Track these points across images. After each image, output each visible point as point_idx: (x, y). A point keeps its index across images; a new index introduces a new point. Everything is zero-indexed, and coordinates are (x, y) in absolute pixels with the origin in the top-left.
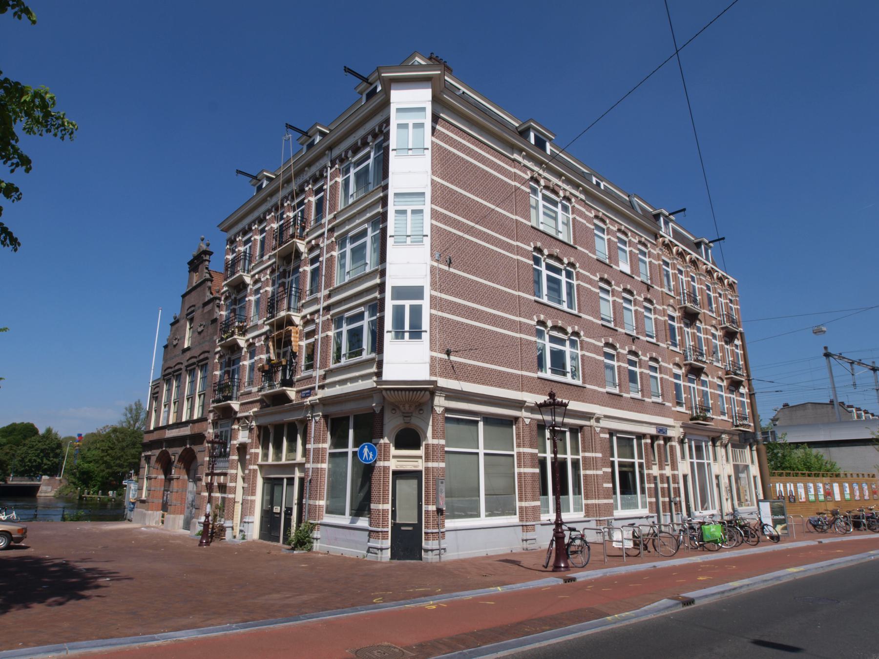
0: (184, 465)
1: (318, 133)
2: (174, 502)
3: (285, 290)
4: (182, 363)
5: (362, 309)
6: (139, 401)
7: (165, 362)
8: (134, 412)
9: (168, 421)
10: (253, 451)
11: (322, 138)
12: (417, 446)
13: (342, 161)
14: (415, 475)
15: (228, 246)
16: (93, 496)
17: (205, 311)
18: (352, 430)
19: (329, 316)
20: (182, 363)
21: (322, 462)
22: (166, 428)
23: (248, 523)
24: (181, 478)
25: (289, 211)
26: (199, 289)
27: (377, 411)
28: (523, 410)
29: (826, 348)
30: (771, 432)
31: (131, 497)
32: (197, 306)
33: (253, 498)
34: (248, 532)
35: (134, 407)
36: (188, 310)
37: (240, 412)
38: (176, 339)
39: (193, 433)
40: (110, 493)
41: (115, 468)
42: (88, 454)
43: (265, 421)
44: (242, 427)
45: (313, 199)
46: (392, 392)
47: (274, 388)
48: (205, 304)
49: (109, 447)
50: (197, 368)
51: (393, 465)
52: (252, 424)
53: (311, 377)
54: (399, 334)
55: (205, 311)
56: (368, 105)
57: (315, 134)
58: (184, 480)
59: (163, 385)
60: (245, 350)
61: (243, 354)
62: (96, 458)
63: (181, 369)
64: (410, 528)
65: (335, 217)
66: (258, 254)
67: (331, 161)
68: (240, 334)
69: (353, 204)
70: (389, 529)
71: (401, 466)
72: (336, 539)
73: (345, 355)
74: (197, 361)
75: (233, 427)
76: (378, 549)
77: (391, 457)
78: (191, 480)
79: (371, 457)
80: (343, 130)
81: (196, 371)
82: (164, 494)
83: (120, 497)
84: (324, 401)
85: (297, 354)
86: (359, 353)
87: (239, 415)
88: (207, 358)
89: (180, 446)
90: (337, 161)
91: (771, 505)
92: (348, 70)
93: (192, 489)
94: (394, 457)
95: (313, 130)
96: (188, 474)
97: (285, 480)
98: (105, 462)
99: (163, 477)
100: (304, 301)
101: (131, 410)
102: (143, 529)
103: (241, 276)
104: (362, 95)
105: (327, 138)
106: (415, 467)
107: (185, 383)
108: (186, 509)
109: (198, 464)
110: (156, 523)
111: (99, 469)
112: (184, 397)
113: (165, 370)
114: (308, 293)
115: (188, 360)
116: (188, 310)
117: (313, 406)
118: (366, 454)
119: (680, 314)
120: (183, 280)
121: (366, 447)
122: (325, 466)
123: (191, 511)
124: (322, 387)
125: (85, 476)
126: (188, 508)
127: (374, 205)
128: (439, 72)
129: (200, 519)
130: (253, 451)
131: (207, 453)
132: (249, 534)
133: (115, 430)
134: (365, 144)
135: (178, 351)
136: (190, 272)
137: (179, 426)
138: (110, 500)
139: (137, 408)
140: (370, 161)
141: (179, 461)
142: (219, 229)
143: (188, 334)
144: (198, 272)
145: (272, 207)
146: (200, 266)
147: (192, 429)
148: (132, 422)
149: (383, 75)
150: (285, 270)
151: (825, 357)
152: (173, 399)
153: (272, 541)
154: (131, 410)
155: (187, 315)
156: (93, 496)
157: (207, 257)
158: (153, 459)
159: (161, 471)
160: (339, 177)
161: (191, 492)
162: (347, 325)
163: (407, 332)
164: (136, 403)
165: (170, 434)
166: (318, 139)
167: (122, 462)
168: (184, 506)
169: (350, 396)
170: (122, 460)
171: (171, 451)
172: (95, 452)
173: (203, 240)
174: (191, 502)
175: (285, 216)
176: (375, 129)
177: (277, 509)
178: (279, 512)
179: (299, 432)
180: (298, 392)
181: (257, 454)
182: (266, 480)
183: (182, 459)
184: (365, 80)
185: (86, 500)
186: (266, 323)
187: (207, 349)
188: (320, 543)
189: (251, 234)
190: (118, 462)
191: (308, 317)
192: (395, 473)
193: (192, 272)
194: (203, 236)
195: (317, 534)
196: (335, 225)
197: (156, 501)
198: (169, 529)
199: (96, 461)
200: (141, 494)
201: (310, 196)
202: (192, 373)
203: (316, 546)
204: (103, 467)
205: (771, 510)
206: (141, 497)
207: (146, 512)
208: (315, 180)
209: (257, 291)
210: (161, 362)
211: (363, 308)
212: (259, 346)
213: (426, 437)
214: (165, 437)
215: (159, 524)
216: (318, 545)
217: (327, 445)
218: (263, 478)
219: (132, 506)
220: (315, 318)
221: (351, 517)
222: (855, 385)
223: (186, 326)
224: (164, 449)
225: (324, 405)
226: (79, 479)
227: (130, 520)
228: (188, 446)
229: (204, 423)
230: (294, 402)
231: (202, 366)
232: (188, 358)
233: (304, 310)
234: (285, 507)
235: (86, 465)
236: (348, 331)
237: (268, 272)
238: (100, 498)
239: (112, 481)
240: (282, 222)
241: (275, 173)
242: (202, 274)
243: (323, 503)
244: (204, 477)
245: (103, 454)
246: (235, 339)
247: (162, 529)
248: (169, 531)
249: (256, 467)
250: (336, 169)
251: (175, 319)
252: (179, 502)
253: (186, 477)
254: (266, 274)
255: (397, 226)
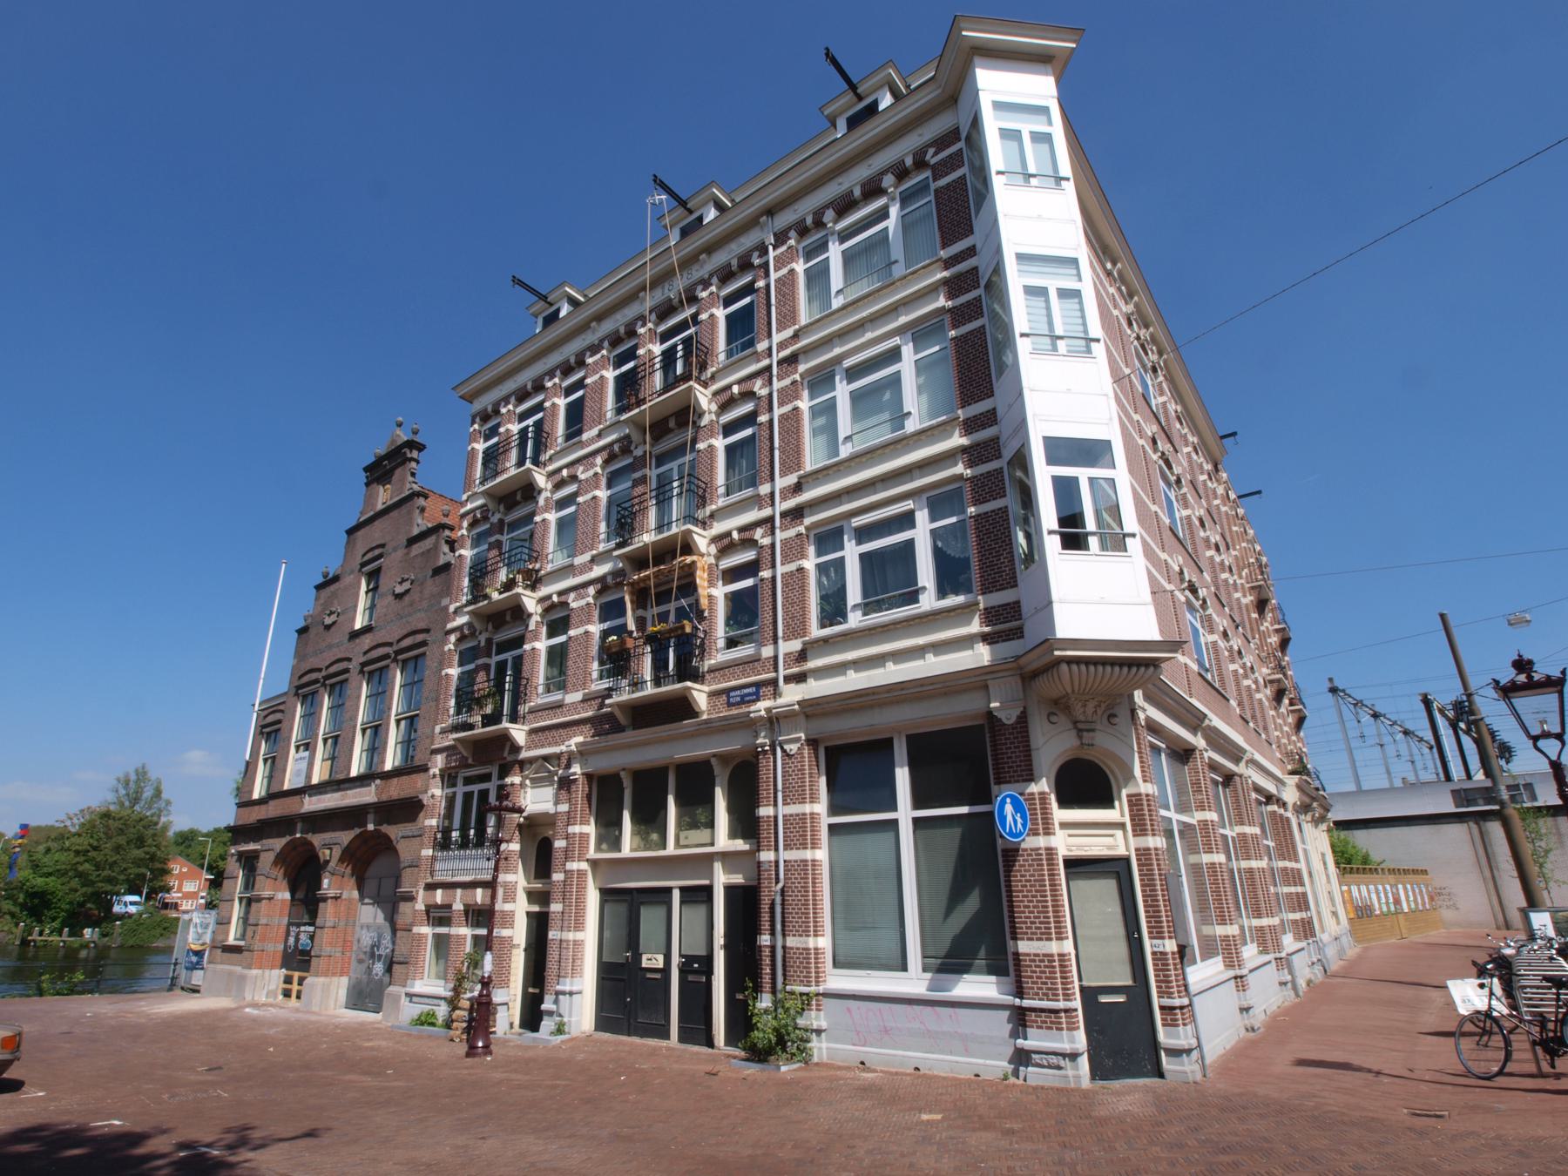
0: (353, 870)
1: (566, 299)
2: (327, 950)
3: (501, 554)
4: (349, 660)
5: (908, 505)
6: (143, 768)
7: (299, 662)
8: (132, 785)
9: (309, 776)
10: (575, 829)
11: (572, 309)
12: (1106, 800)
13: (803, 232)
14: (1114, 868)
15: (476, 426)
16: (50, 939)
17: (412, 554)
18: (906, 769)
19: (802, 529)
20: (349, 660)
21: (814, 846)
22: (304, 792)
23: (571, 994)
24: (344, 897)
25: (651, 341)
26: (395, 514)
27: (1009, 717)
28: (1199, 734)
29: (1331, 680)
30: (1524, 785)
31: (190, 940)
32: (389, 548)
33: (579, 936)
34: (570, 1016)
35: (133, 777)
36: (364, 555)
37: (529, 748)
38: (332, 613)
39: (384, 798)
40: (87, 932)
41: (100, 885)
42: (45, 860)
43: (605, 763)
44: (532, 780)
45: (562, 402)
46: (1083, 667)
47: (642, 689)
48: (412, 541)
49: (90, 845)
50: (392, 665)
51: (1064, 844)
52: (572, 770)
53: (759, 660)
54: (1073, 541)
55: (412, 554)
56: (899, 108)
57: (705, 204)
58: (350, 900)
59: (296, 707)
60: (536, 618)
61: (532, 626)
62: (64, 867)
63: (347, 671)
64: (1121, 999)
65: (796, 336)
66: (478, 476)
67: (775, 235)
68: (528, 585)
69: (843, 308)
70: (1077, 1003)
71: (1079, 847)
72: (886, 1031)
73: (855, 607)
74: (323, 677)
75: (508, 780)
76: (1064, 1055)
77: (1057, 826)
78: (367, 901)
79: (1019, 826)
80: (792, 184)
81: (391, 672)
82: (288, 934)
83: (107, 939)
84: (811, 709)
85: (706, 614)
86: (913, 597)
87: (524, 755)
88: (424, 644)
89: (280, 835)
90: (793, 234)
91: (1552, 918)
92: (517, 281)
93: (371, 921)
94: (1064, 825)
95: (558, 293)
96: (360, 887)
97: (676, 895)
98: (80, 875)
99: (287, 895)
100: (714, 507)
101: (127, 783)
102: (247, 1010)
103: (529, 470)
104: (537, 317)
105: (728, 215)
106: (1110, 847)
107: (359, 697)
108: (354, 963)
109: (402, 865)
110: (267, 996)
111: (66, 888)
112: (355, 727)
113: (300, 677)
114: (722, 490)
115: (365, 653)
116: (364, 555)
117: (774, 721)
118: (1009, 818)
119: (1252, 598)
120: (353, 499)
121: (1008, 800)
122: (822, 854)
123: (369, 969)
124: (800, 678)
125: (36, 901)
126: (360, 961)
127: (882, 315)
128: (1074, 45)
129: (413, 987)
130: (575, 829)
131: (427, 839)
132: (573, 1019)
133: (106, 815)
134: (873, 190)
135: (338, 635)
136: (367, 485)
137: (342, 786)
138: (85, 946)
139: (138, 779)
140: (892, 223)
141: (341, 860)
142: (456, 395)
143: (363, 602)
144: (389, 483)
145: (711, 276)
146: (398, 472)
147: (379, 791)
148: (127, 804)
149: (964, 33)
150: (501, 521)
151: (1330, 694)
152: (262, 753)
153: (642, 1037)
154: (127, 783)
155: (363, 565)
156: (50, 939)
157: (415, 454)
158: (266, 860)
159: (285, 882)
160: (607, 369)
161: (368, 927)
162: (724, 585)
163: (1093, 534)
164: (137, 770)
165: (311, 804)
166: (711, 214)
167: (114, 874)
168: (350, 958)
169: (878, 693)
170: (117, 869)
171: (317, 840)
172: (62, 857)
173: (400, 425)
174: (368, 949)
175: (502, 430)
176: (526, 386)
177: (652, 960)
178: (661, 965)
179: (718, 781)
180: (712, 695)
181: (584, 837)
182: (607, 895)
183: (348, 855)
184: (544, 298)
185: (35, 946)
186: (466, 610)
187: (422, 625)
188: (828, 1041)
189: (581, 374)
190: (106, 873)
191: (555, 599)
192: (1071, 863)
193: (375, 485)
194: (400, 419)
195: (817, 1018)
196: (799, 349)
197: (270, 947)
198: (315, 1009)
199: (61, 873)
200: (227, 933)
201: (555, 395)
202: (376, 672)
203: (820, 1049)
204: (75, 883)
205: (1555, 927)
206: (226, 940)
207: (246, 972)
208: (567, 370)
209: (562, 504)
210: (289, 661)
211: (911, 502)
212: (581, 608)
213: (1130, 777)
214: (303, 811)
215: (276, 997)
216: (824, 1045)
217: (821, 807)
218: (600, 890)
219: (194, 959)
220: (570, 601)
221: (929, 975)
222: (1363, 737)
223: (359, 588)
224: (298, 835)
225: (807, 716)
226: (23, 906)
227: (195, 990)
228: (371, 827)
229: (418, 779)
230: (705, 717)
231: (332, 686)
232: (367, 648)
233: (715, 524)
234: (681, 956)
235: (40, 881)
236: (726, 595)
237: (599, 460)
238: (64, 941)
239: (91, 909)
240: (495, 440)
241: (586, 292)
242: (404, 484)
243: (824, 942)
244: (421, 892)
245: (77, 859)
246: (518, 595)
247: (297, 1010)
248: (314, 1013)
249: (584, 866)
250: (603, 356)
251: (325, 576)
252: (340, 949)
253: (356, 894)
254: (594, 465)
255: (1032, 318)
